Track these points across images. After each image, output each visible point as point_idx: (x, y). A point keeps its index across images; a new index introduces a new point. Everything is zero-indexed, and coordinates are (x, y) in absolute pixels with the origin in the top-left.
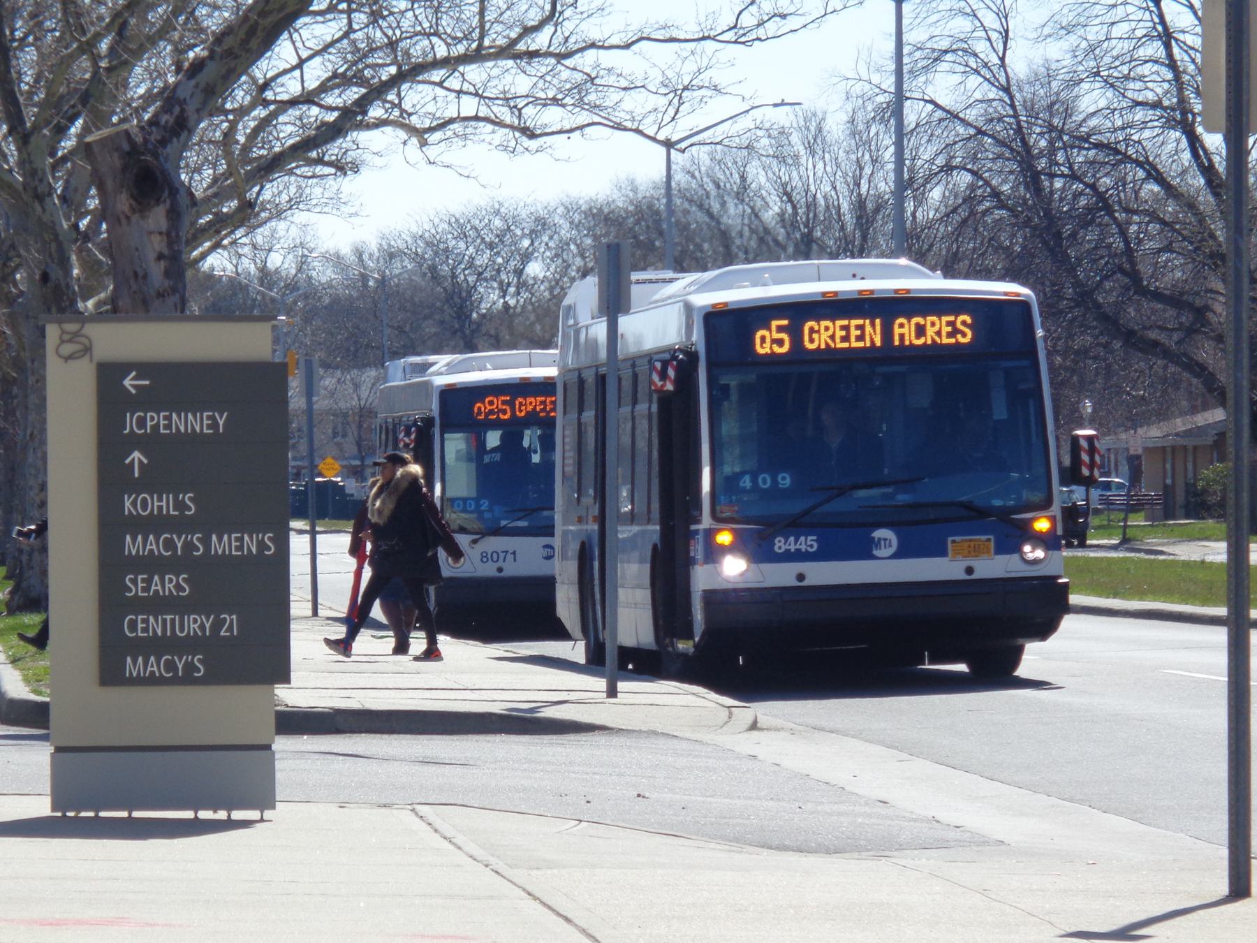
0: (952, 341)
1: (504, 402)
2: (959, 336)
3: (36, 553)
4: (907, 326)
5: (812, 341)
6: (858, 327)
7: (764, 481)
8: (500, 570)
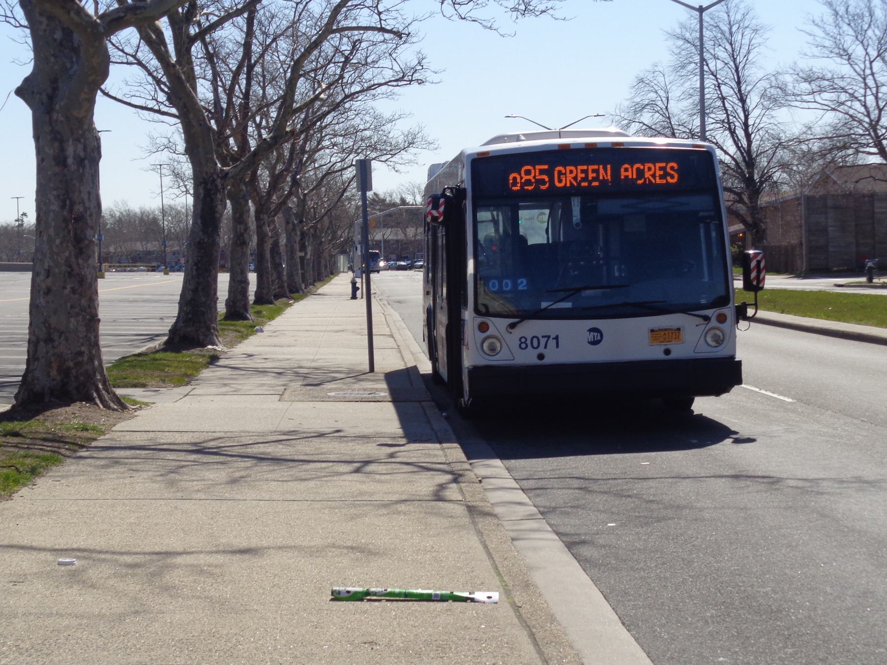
0: (664, 181)
1: (542, 172)
2: (668, 178)
3: (42, 343)
4: (630, 170)
5: (560, 181)
6: (593, 171)
7: (507, 285)
8: (541, 357)
